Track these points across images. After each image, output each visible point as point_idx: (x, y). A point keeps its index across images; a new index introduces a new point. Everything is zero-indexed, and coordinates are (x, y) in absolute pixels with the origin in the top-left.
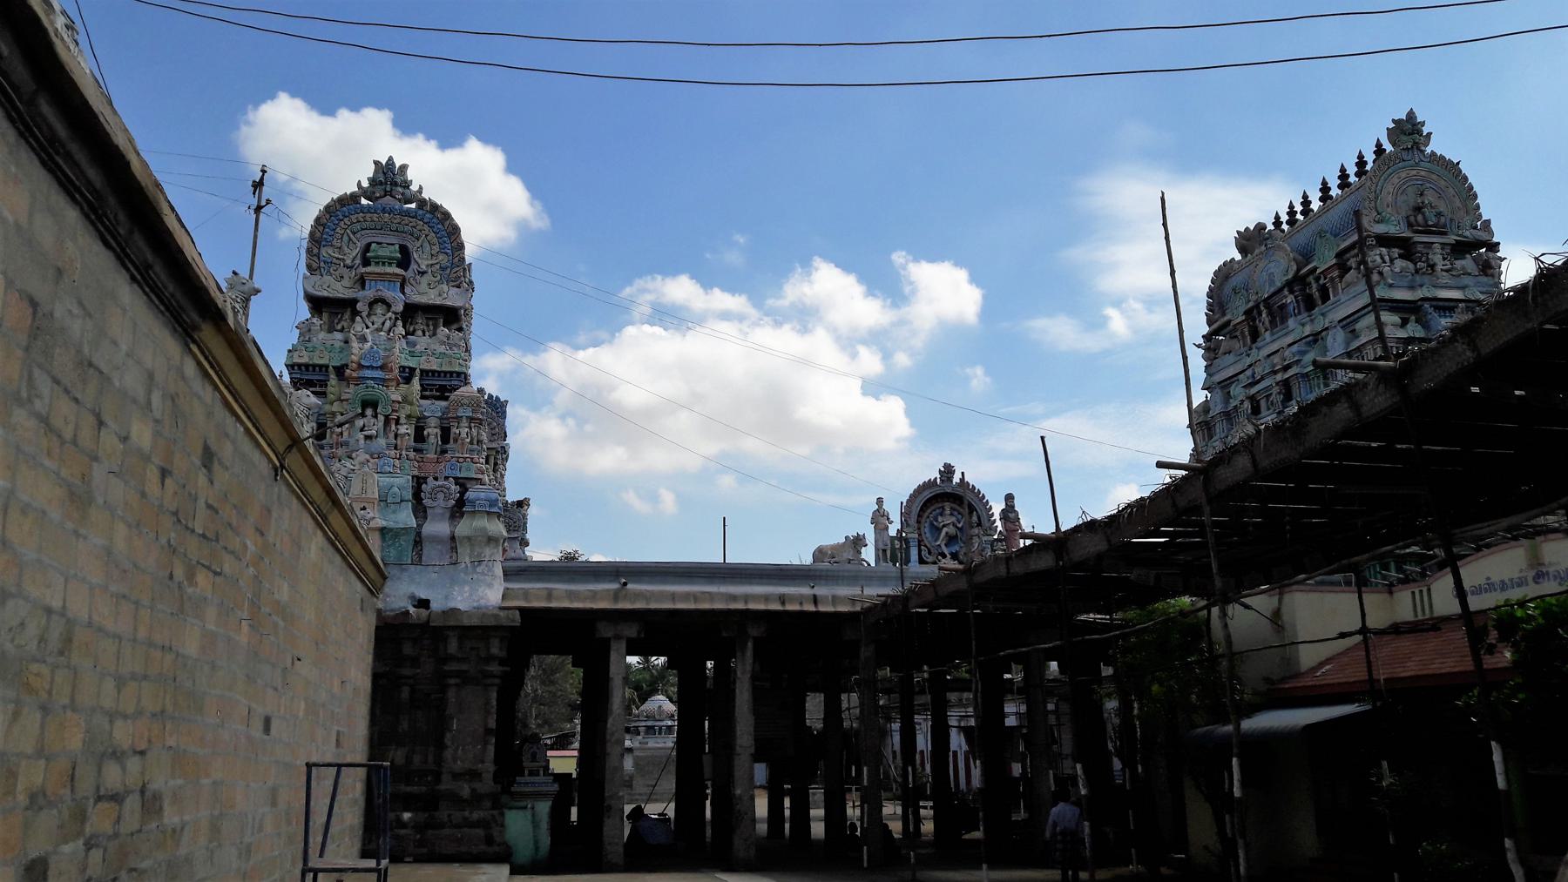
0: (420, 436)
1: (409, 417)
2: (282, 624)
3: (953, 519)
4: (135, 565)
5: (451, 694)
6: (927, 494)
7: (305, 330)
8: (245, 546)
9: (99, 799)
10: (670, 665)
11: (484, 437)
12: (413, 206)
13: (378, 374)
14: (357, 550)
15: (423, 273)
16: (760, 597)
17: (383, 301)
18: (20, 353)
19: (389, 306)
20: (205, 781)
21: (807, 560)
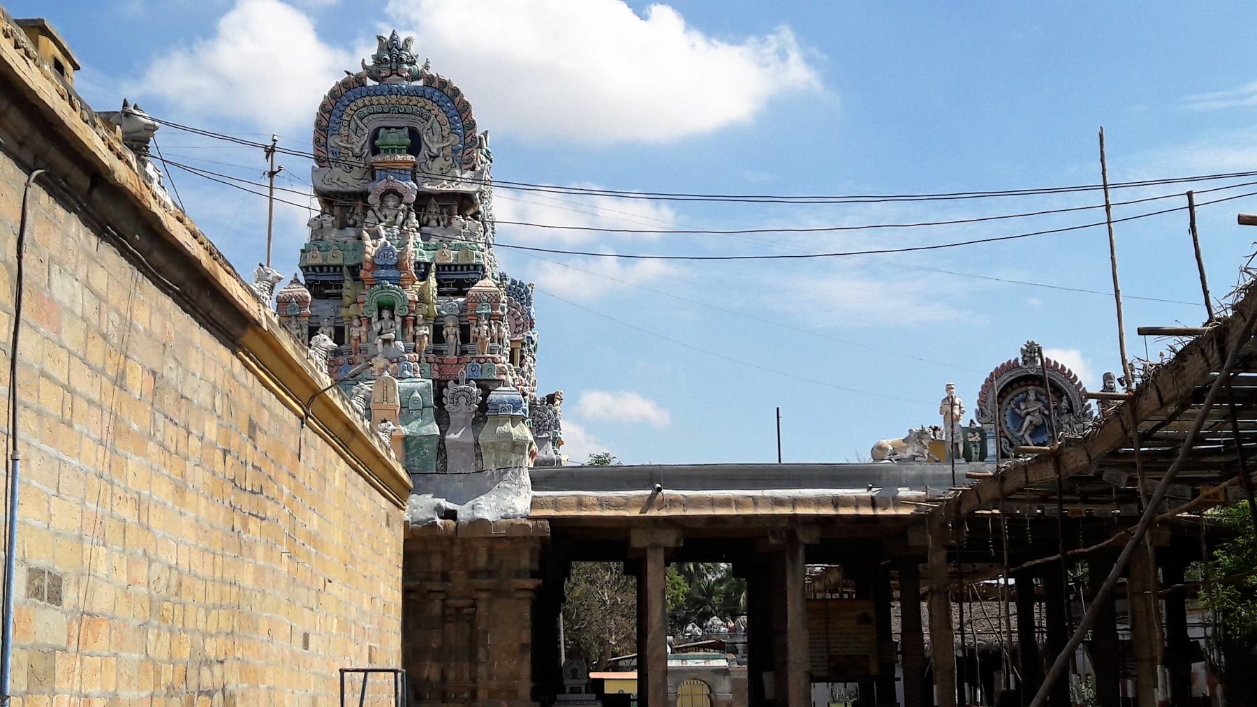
0: (438, 336)
1: (426, 317)
2: (313, 550)
3: (1040, 405)
4: (212, 527)
5: (482, 608)
6: (1007, 378)
7: (317, 228)
8: (282, 492)
9: (200, 693)
10: (735, 572)
11: (506, 332)
12: (420, 83)
13: (392, 273)
14: (379, 469)
15: (433, 158)
16: (810, 500)
17: (394, 192)
18: (149, 408)
19: (400, 196)
20: (262, 686)
21: (867, 458)
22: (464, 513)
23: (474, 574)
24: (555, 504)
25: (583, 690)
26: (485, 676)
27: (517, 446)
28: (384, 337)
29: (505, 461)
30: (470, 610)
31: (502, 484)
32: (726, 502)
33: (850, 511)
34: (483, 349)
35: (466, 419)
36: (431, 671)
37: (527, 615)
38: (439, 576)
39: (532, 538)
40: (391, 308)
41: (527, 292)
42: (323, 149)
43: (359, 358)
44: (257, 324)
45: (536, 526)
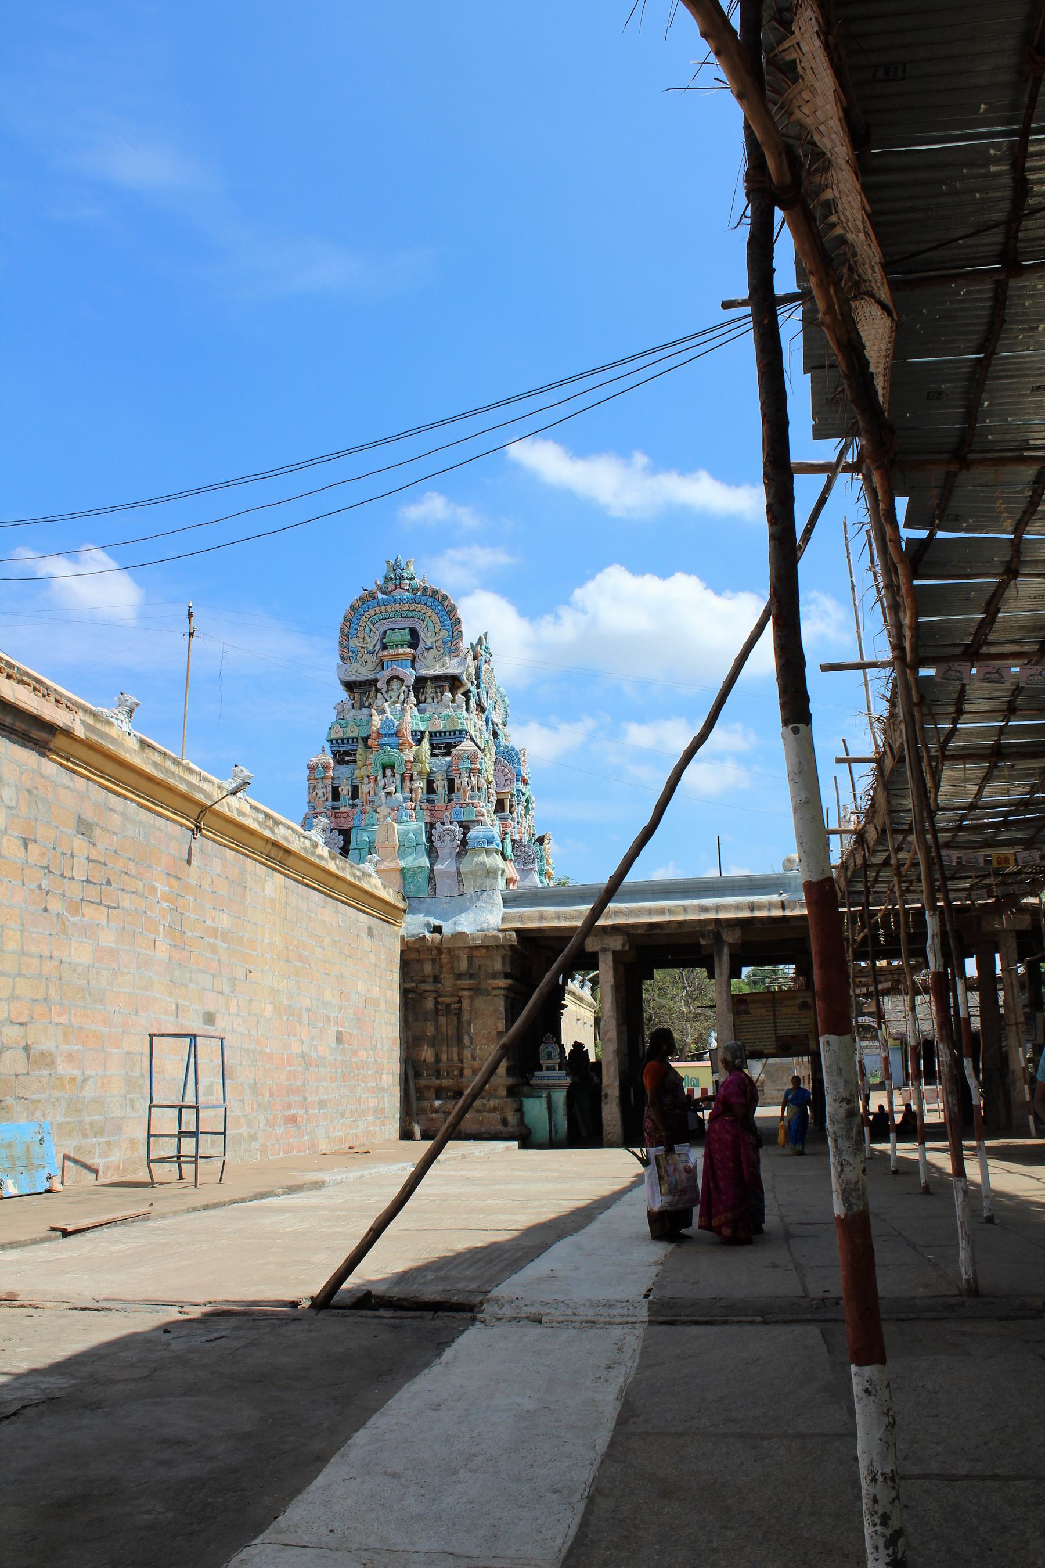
0: (430, 789)
5: (466, 1004)
13: (391, 740)
16: (731, 907)
17: (397, 678)
19: (402, 681)
22: (448, 929)
23: (459, 976)
24: (522, 918)
25: (557, 1067)
26: (470, 1058)
27: (491, 873)
28: (387, 790)
29: (481, 886)
30: (457, 1006)
31: (479, 904)
32: (661, 911)
33: (764, 913)
34: (465, 796)
35: (451, 853)
36: (427, 1054)
37: (502, 1009)
38: (431, 979)
39: (503, 946)
40: (392, 767)
41: (517, 754)
42: (346, 650)
43: (368, 808)
44: (67, 733)
45: (505, 937)
